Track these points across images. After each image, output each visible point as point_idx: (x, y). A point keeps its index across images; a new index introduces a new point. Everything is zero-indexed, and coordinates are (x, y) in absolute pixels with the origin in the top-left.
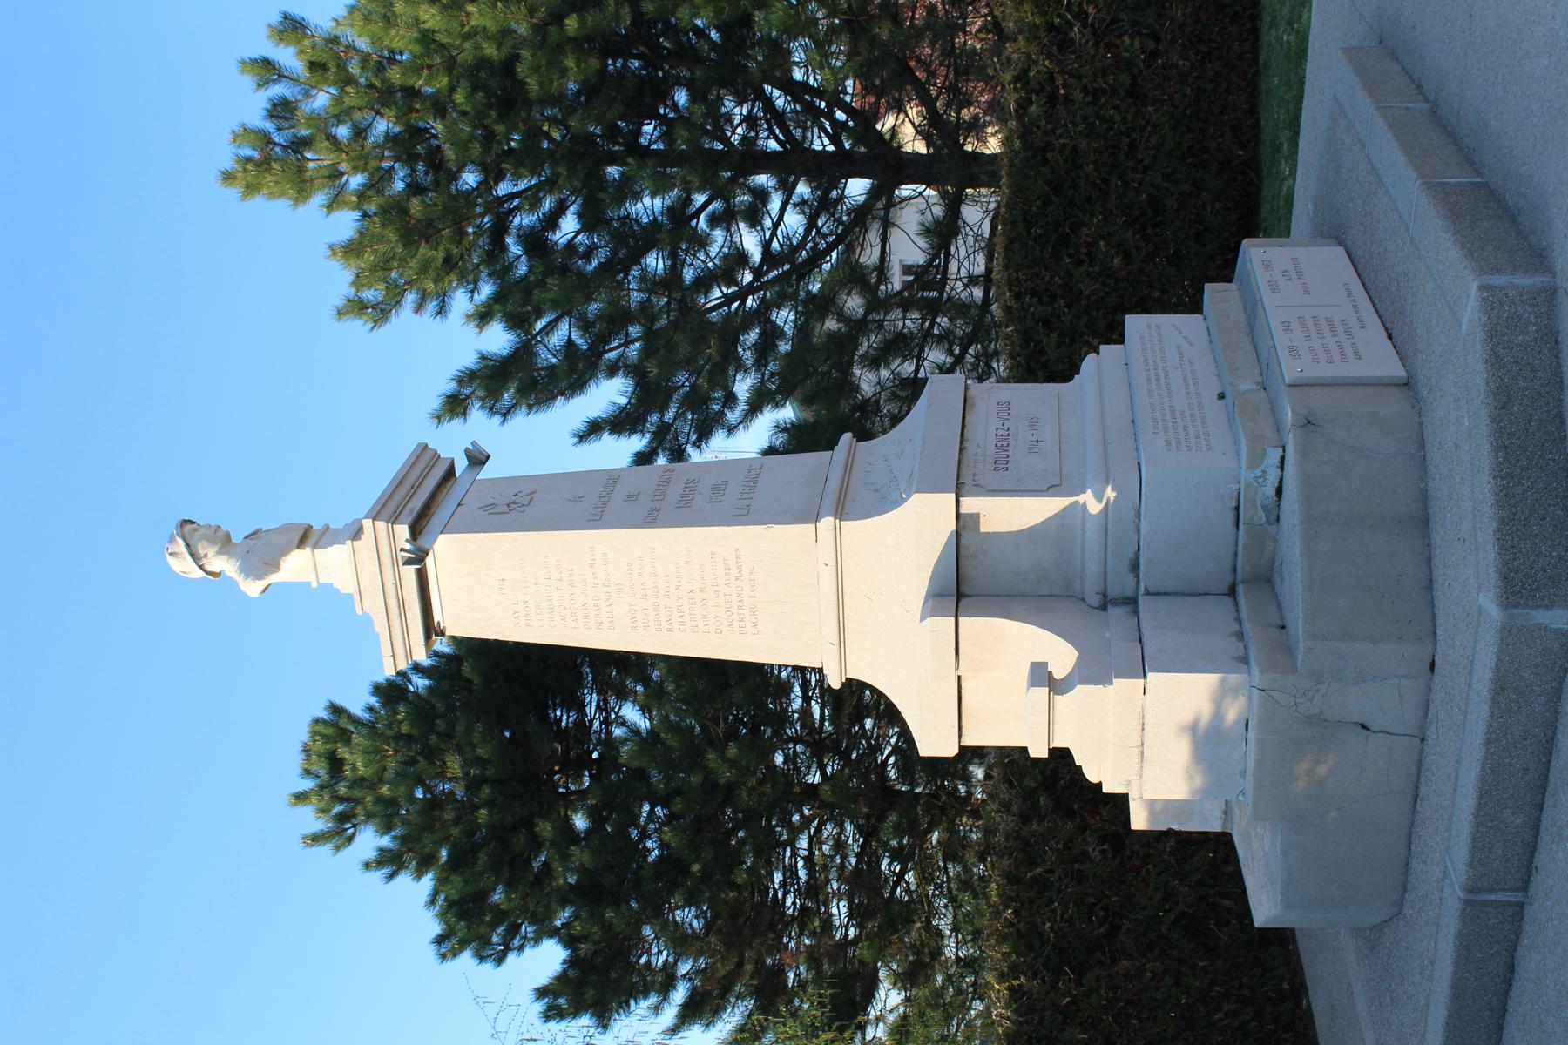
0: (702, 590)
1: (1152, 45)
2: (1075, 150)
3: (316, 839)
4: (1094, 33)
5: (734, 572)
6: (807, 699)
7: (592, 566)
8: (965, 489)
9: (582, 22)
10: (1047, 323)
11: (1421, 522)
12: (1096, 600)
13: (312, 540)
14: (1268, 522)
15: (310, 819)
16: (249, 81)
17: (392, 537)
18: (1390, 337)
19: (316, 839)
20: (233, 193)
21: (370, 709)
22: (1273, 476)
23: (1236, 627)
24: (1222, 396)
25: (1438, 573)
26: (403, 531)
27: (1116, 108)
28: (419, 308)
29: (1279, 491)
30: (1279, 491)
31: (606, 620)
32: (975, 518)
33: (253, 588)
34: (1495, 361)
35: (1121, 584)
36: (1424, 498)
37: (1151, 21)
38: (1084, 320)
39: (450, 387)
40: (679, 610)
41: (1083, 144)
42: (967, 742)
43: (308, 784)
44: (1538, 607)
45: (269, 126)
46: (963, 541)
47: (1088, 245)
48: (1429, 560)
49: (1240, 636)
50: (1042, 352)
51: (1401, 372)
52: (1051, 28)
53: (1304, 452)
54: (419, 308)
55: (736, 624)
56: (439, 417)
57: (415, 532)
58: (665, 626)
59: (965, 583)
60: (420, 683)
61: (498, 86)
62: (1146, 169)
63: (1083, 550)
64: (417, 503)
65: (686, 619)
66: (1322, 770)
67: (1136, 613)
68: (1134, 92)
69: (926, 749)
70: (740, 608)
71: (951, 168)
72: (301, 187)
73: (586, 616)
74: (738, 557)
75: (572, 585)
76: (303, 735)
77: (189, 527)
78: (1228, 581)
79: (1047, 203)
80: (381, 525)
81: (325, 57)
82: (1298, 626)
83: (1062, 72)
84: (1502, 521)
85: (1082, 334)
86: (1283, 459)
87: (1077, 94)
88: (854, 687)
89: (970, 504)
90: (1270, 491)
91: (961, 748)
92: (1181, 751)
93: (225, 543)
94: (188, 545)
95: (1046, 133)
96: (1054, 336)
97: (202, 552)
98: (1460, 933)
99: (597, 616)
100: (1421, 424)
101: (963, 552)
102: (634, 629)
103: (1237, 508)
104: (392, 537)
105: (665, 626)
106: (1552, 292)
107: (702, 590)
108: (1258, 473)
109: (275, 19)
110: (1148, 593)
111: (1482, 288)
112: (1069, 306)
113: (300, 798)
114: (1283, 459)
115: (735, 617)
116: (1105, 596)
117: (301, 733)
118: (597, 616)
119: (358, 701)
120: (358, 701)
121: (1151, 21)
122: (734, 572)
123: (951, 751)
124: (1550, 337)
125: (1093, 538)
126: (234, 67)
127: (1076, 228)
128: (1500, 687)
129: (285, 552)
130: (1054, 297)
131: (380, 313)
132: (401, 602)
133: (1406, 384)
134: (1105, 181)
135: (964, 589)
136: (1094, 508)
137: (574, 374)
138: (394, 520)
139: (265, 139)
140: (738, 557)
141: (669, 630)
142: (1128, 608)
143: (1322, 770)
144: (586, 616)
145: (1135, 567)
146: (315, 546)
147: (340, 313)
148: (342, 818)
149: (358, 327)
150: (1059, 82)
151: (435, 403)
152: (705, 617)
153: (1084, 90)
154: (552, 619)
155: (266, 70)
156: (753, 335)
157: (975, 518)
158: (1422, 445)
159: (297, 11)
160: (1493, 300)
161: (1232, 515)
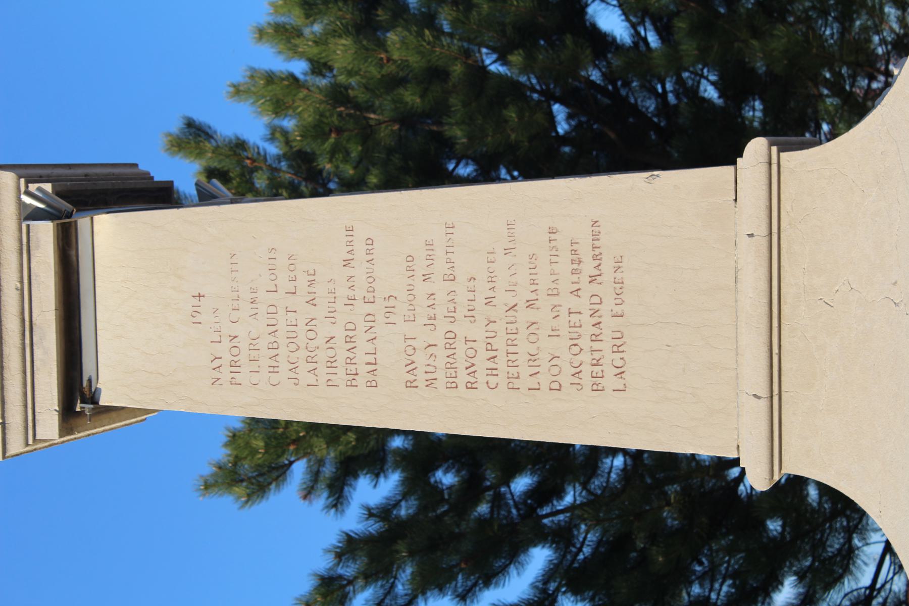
0: (530, 305)
5: (588, 268)
6: (720, 589)
7: (347, 263)
28: (308, 493)
31: (363, 369)
39: (323, 563)
40: (489, 347)
54: (308, 493)
55: (586, 369)
58: (463, 378)
65: (501, 363)
70: (595, 338)
73: (331, 362)
74: (596, 237)
75: (311, 302)
81: (226, 164)
99: (350, 361)
102: (410, 385)
105: (463, 378)
107: (530, 305)
109: (176, 126)
115: (586, 357)
118: (350, 361)
122: (588, 268)
140: (596, 237)
141: (470, 386)
144: (331, 362)
147: (208, 486)
149: (226, 503)
152: (533, 358)
154: (274, 370)
156: (725, 565)
159: (201, 117)
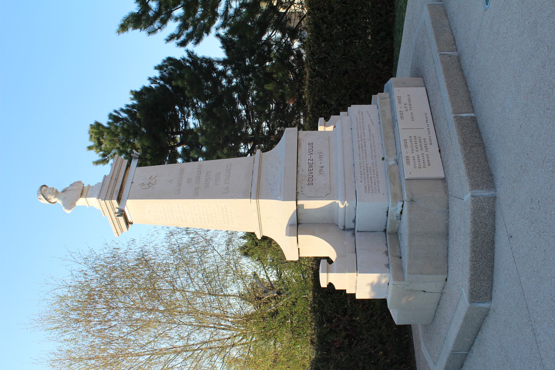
3: (97, 163)
8: (299, 196)
11: (446, 235)
12: (342, 228)
13: (85, 194)
14: (397, 219)
15: (96, 156)
18: (440, 151)
19: (97, 163)
21: (109, 123)
22: (400, 209)
24: (383, 159)
25: (451, 254)
26: (115, 202)
29: (401, 213)
30: (401, 213)
32: (303, 205)
33: (69, 212)
35: (350, 225)
36: (447, 227)
38: (335, 19)
42: (301, 255)
43: (91, 144)
44: (480, 302)
46: (298, 211)
48: (448, 248)
49: (386, 244)
50: (321, 30)
53: (410, 211)
56: (118, 32)
57: (119, 200)
59: (299, 224)
60: (124, 115)
63: (338, 214)
66: (410, 299)
67: (354, 234)
69: (288, 258)
76: (88, 136)
77: (44, 188)
78: (384, 228)
80: (107, 201)
85: (334, 24)
86: (403, 205)
88: (264, 238)
89: (300, 202)
90: (399, 212)
91: (299, 257)
93: (56, 193)
94: (44, 196)
96: (325, 25)
97: (49, 198)
98: (449, 358)
100: (448, 200)
101: (299, 213)
103: (387, 212)
106: (495, 198)
108: (395, 208)
110: (358, 231)
112: (330, 14)
113: (90, 148)
114: (403, 205)
116: (344, 227)
117: (88, 128)
119: (105, 121)
120: (105, 121)
123: (296, 259)
125: (341, 214)
128: (466, 318)
130: (325, 10)
132: (118, 176)
133: (444, 180)
135: (299, 222)
136: (341, 206)
138: (111, 198)
143: (410, 299)
145: (354, 221)
146: (86, 197)
148: (104, 155)
151: (117, 27)
157: (303, 205)
158: (448, 208)
160: (475, 199)
161: (386, 214)
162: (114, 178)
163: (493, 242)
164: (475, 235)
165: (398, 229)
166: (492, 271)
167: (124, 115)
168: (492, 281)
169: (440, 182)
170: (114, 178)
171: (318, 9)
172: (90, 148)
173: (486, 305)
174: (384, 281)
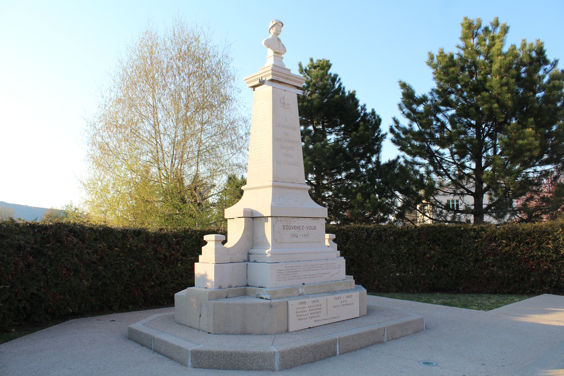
1: (490, 265)
2: (460, 244)
3: (300, 65)
4: (494, 249)
8: (275, 219)
9: (496, 108)
10: (412, 237)
11: (244, 333)
12: (250, 252)
13: (277, 55)
15: (306, 64)
16: (492, 20)
17: (268, 75)
18: (310, 328)
19: (300, 65)
20: (462, 21)
21: (330, 74)
22: (264, 297)
23: (233, 286)
24: (304, 284)
26: (270, 77)
27: (472, 256)
29: (262, 298)
30: (262, 298)
34: (254, 354)
35: (252, 258)
36: (250, 334)
37: (497, 265)
41: (461, 246)
42: (228, 220)
43: (315, 61)
45: (482, 28)
47: (434, 248)
49: (237, 287)
51: (290, 330)
52: (495, 237)
53: (263, 304)
60: (337, 86)
61: (479, 88)
62: (455, 263)
64: (281, 80)
66: (194, 305)
68: (477, 260)
71: (478, 212)
72: (465, 38)
77: (281, 25)
78: (250, 285)
79: (445, 237)
80: (271, 72)
82: (225, 301)
83: (482, 241)
84: (213, 352)
87: (476, 245)
88: (242, 192)
89: (270, 219)
90: (262, 296)
91: (227, 219)
92: (202, 272)
93: (277, 34)
95: (466, 236)
96: (407, 240)
104: (268, 75)
106: (273, 370)
109: (508, 25)
111: (274, 353)
112: (416, 243)
113: (311, 60)
119: (332, 71)
120: (332, 71)
121: (497, 265)
124: (261, 369)
126: (496, 16)
127: (439, 245)
129: (272, 49)
130: (419, 239)
131: (430, 64)
133: (287, 331)
134: (452, 252)
136: (267, 251)
137: (413, 116)
138: (273, 74)
139: (479, 27)
142: (246, 259)
143: (194, 305)
145: (255, 262)
146: (274, 56)
148: (306, 70)
149: (426, 58)
150: (479, 240)
151: (403, 81)
153: (477, 247)
155: (496, 24)
158: (265, 334)
161: (261, 286)
162: (288, 77)
163: (239, 369)
164: (244, 355)
165: (249, 296)
166: (216, 368)
167: (337, 86)
168: (208, 368)
169: (286, 328)
170: (288, 77)
171: (419, 234)
172: (311, 60)
173: (189, 364)
174: (209, 284)
